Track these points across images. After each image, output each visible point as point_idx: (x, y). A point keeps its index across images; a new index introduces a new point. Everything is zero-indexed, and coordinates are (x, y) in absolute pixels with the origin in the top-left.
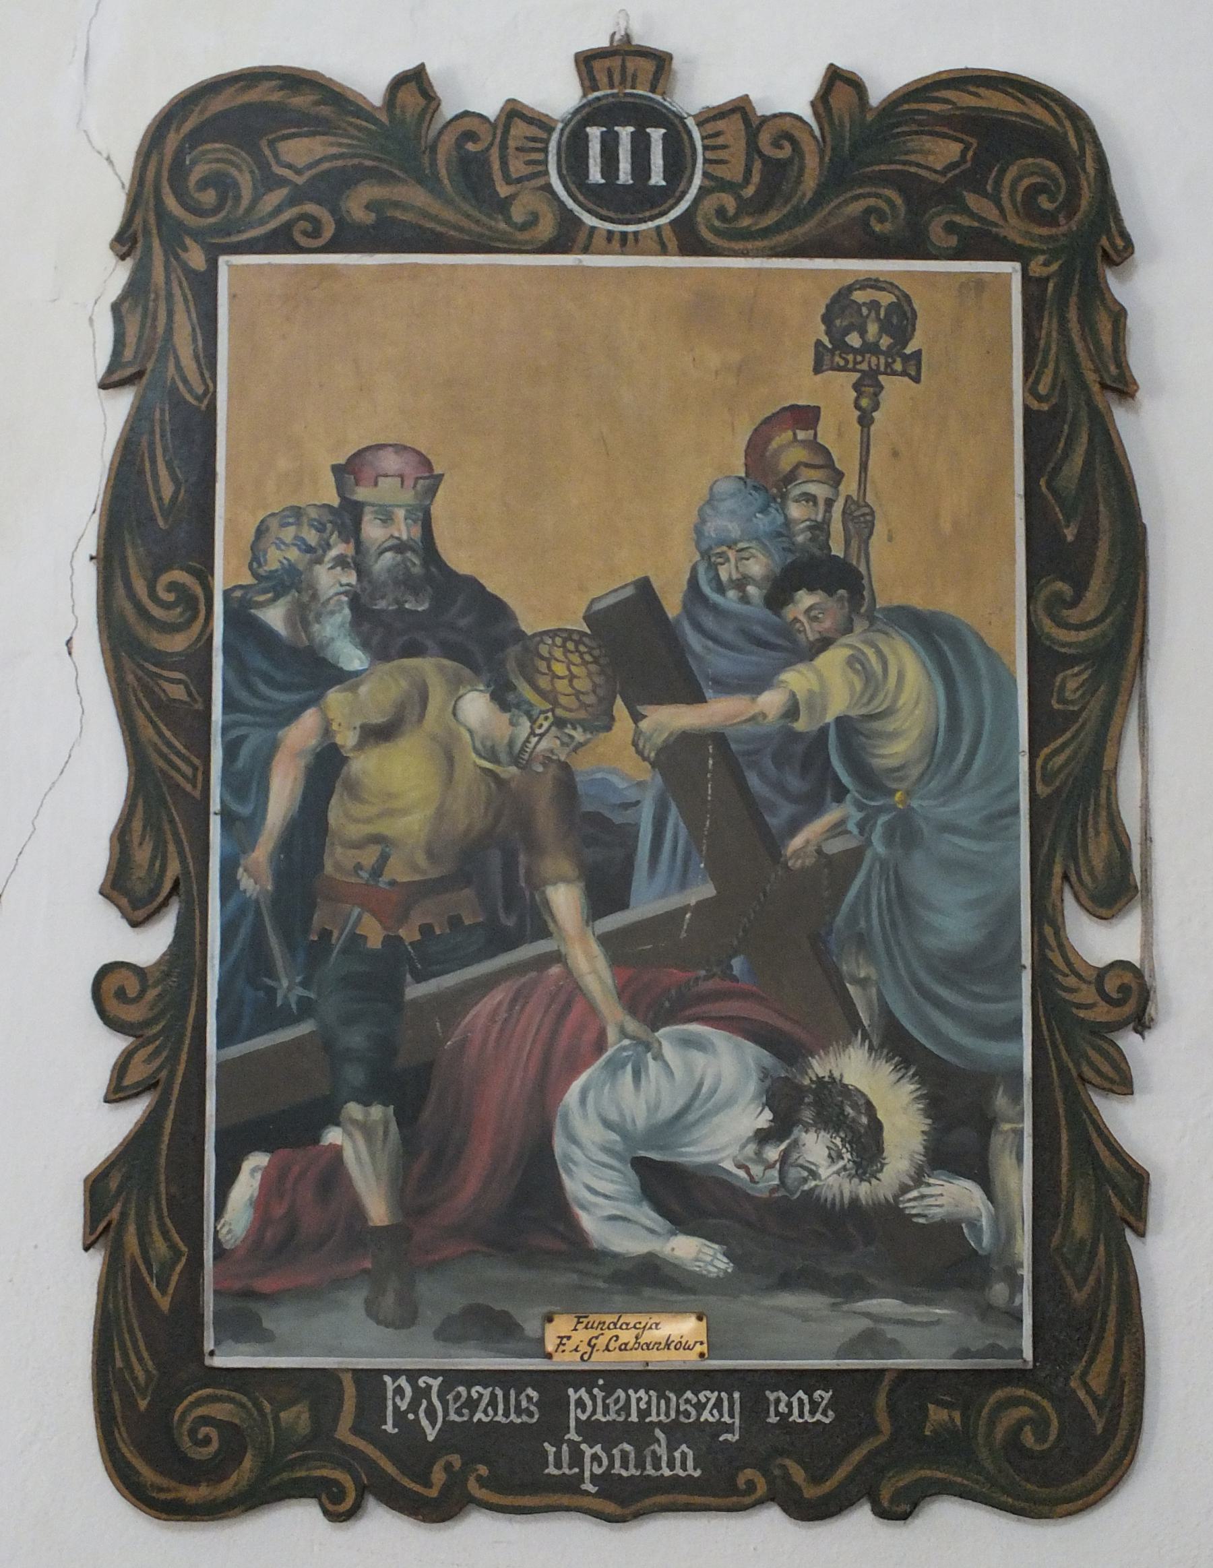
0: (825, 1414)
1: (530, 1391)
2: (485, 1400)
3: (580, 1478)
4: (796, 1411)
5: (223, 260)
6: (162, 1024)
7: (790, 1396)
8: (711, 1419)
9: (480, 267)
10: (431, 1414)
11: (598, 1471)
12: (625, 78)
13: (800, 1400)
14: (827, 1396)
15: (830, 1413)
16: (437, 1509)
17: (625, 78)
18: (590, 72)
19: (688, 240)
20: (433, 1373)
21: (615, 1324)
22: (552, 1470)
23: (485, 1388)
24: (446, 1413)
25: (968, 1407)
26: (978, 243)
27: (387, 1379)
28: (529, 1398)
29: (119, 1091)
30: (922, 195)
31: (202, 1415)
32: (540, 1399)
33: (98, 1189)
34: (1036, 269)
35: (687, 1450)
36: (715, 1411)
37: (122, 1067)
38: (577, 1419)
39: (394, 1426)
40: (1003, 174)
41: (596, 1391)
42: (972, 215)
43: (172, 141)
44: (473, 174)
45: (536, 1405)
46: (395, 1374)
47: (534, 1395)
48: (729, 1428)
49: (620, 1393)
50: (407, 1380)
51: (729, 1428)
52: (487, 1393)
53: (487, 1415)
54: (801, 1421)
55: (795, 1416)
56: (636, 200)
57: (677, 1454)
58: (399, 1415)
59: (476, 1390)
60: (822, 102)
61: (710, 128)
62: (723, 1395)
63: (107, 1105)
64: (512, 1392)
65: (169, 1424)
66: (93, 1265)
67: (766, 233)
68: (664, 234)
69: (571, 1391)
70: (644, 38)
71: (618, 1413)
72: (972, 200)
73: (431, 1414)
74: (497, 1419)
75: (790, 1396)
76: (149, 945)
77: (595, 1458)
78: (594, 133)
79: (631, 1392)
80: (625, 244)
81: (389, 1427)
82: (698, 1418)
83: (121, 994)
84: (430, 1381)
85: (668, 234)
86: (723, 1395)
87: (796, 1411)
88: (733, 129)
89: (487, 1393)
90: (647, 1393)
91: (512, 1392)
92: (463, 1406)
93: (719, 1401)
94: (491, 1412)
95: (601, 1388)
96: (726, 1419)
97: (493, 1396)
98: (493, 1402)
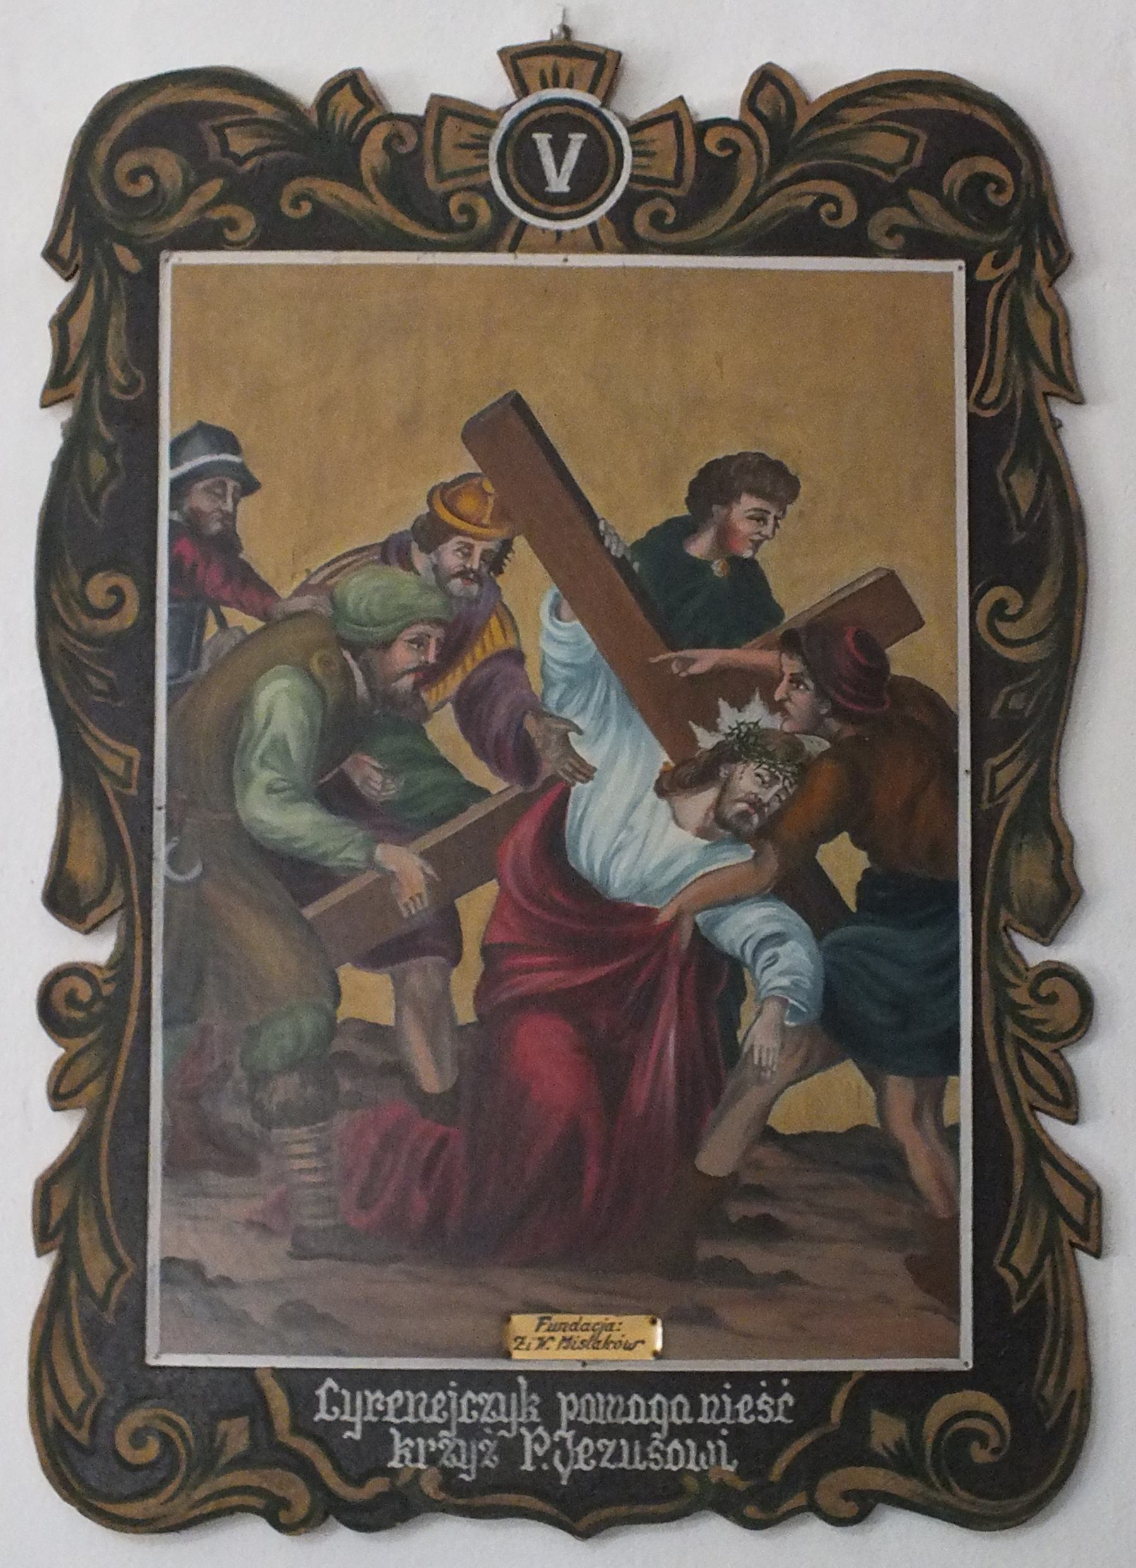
12: (567, 68)
17: (567, 68)
23: (610, 1440)
25: (915, 1418)
26: (923, 244)
29: (60, 1096)
30: (873, 192)
31: (135, 1437)
34: (985, 271)
36: (493, 1413)
38: (534, 1452)
40: (948, 172)
42: (913, 211)
43: (102, 151)
44: (402, 180)
48: (351, 1426)
49: (586, 1441)
50: (545, 1429)
51: (351, 1426)
52: (612, 1445)
58: (536, 1459)
60: (750, 100)
61: (638, 136)
62: (623, 1442)
63: (58, 1114)
66: (34, 1274)
68: (601, 232)
70: (585, 35)
72: (914, 195)
74: (667, 1467)
76: (97, 949)
79: (409, 1393)
83: (72, 1000)
85: (607, 233)
88: (663, 135)
89: (612, 1445)
90: (445, 1393)
92: (592, 1457)
97: (619, 1448)
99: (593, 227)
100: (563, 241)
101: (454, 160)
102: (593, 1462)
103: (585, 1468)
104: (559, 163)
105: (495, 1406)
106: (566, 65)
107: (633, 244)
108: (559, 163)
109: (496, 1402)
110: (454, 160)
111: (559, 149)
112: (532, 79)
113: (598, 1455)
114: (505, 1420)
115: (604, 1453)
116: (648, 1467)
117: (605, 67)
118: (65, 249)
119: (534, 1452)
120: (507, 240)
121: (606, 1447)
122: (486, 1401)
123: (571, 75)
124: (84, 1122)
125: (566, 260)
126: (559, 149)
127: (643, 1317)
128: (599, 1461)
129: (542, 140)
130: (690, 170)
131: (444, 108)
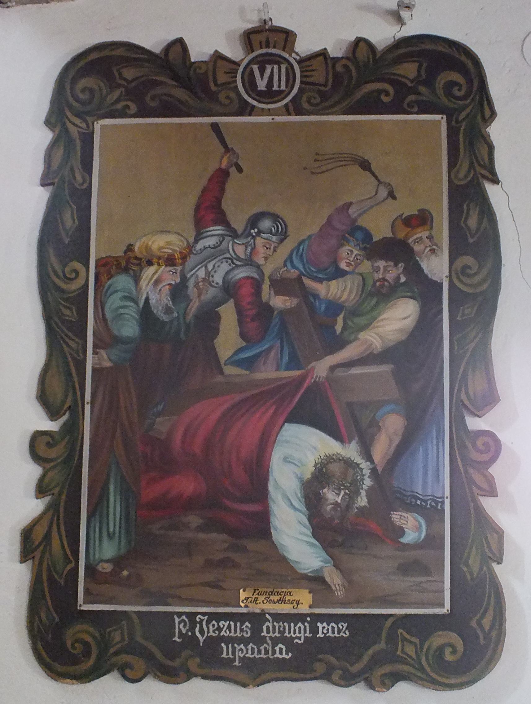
0: (345, 633)
1: (247, 623)
2: (225, 627)
3: (234, 660)
4: (287, 631)
5: (98, 125)
6: (434, 431)
7: (328, 625)
8: (225, 635)
9: (101, 156)
10: (202, 632)
11: (242, 656)
12: (267, 40)
13: (333, 628)
14: (345, 625)
15: (347, 632)
16: (172, 674)
17: (267, 40)
18: (249, 38)
19: (295, 108)
20: (204, 614)
21: (272, 592)
22: (224, 655)
24: (208, 632)
27: (175, 617)
28: (247, 626)
32: (251, 626)
33: (27, 535)
35: (253, 646)
37: (41, 481)
39: (310, 634)
41: (306, 624)
45: (250, 629)
46: (180, 614)
47: (249, 626)
53: (346, 634)
54: (333, 636)
55: (286, 634)
56: (270, 95)
57: (277, 649)
59: (221, 623)
62: (232, 623)
64: (238, 624)
65: (61, 636)
67: (332, 106)
69: (319, 624)
71: (214, 631)
73: (202, 632)
75: (328, 625)
77: (241, 650)
78: (283, 87)
80: (269, 112)
81: (176, 639)
82: (219, 634)
84: (202, 618)
86: (232, 623)
87: (287, 631)
88: (317, 63)
90: (283, 624)
91: (238, 624)
93: (229, 626)
94: (228, 631)
95: (308, 622)
96: (297, 634)
98: (229, 627)
99: (286, 105)
100: (271, 112)
101: (222, 78)
102: (217, 632)
103: (214, 635)
104: (262, 76)
105: (229, 627)
106: (273, 38)
107: (299, 113)
108: (262, 76)
109: (229, 626)
110: (222, 78)
111: (262, 71)
112: (256, 44)
113: (220, 629)
114: (299, 635)
115: (223, 628)
116: (243, 635)
117: (287, 37)
118: (53, 120)
119: (180, 631)
120: (248, 111)
121: (224, 626)
122: (224, 626)
123: (275, 42)
124: (50, 501)
125: (273, 119)
126: (262, 71)
127: (305, 590)
128: (220, 632)
129: (255, 68)
130: (330, 81)
131: (218, 57)
